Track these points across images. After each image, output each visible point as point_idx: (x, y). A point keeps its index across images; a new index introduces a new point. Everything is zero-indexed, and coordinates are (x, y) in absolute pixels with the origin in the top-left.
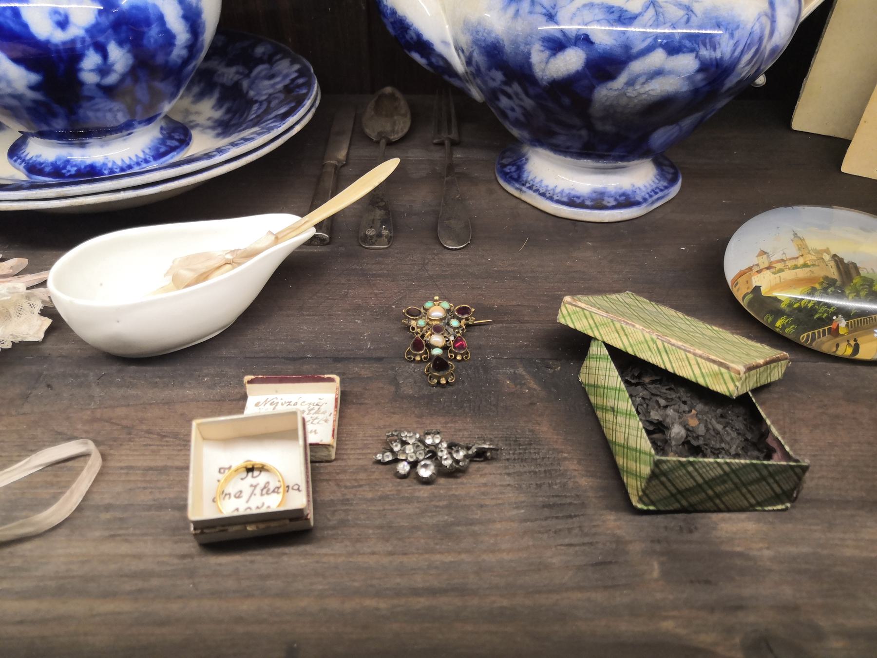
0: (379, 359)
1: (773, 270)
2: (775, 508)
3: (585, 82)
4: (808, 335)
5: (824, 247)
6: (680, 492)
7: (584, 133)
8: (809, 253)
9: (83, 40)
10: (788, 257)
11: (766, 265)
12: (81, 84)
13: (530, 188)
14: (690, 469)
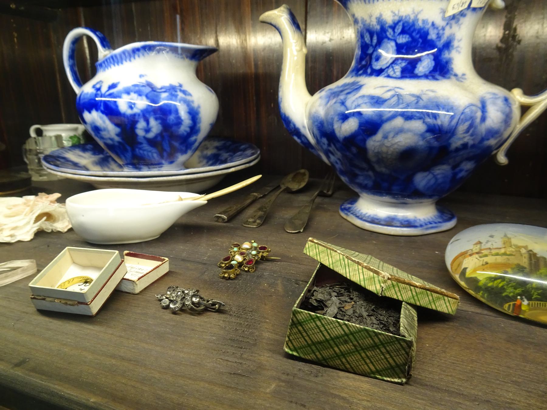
0: (205, 264)
1: (481, 255)
2: (392, 380)
3: (360, 137)
4: (510, 305)
5: (524, 245)
6: (313, 343)
7: (371, 173)
8: (511, 246)
9: (139, 115)
10: (494, 247)
11: (477, 251)
12: (136, 135)
13: (352, 213)
14: (319, 323)
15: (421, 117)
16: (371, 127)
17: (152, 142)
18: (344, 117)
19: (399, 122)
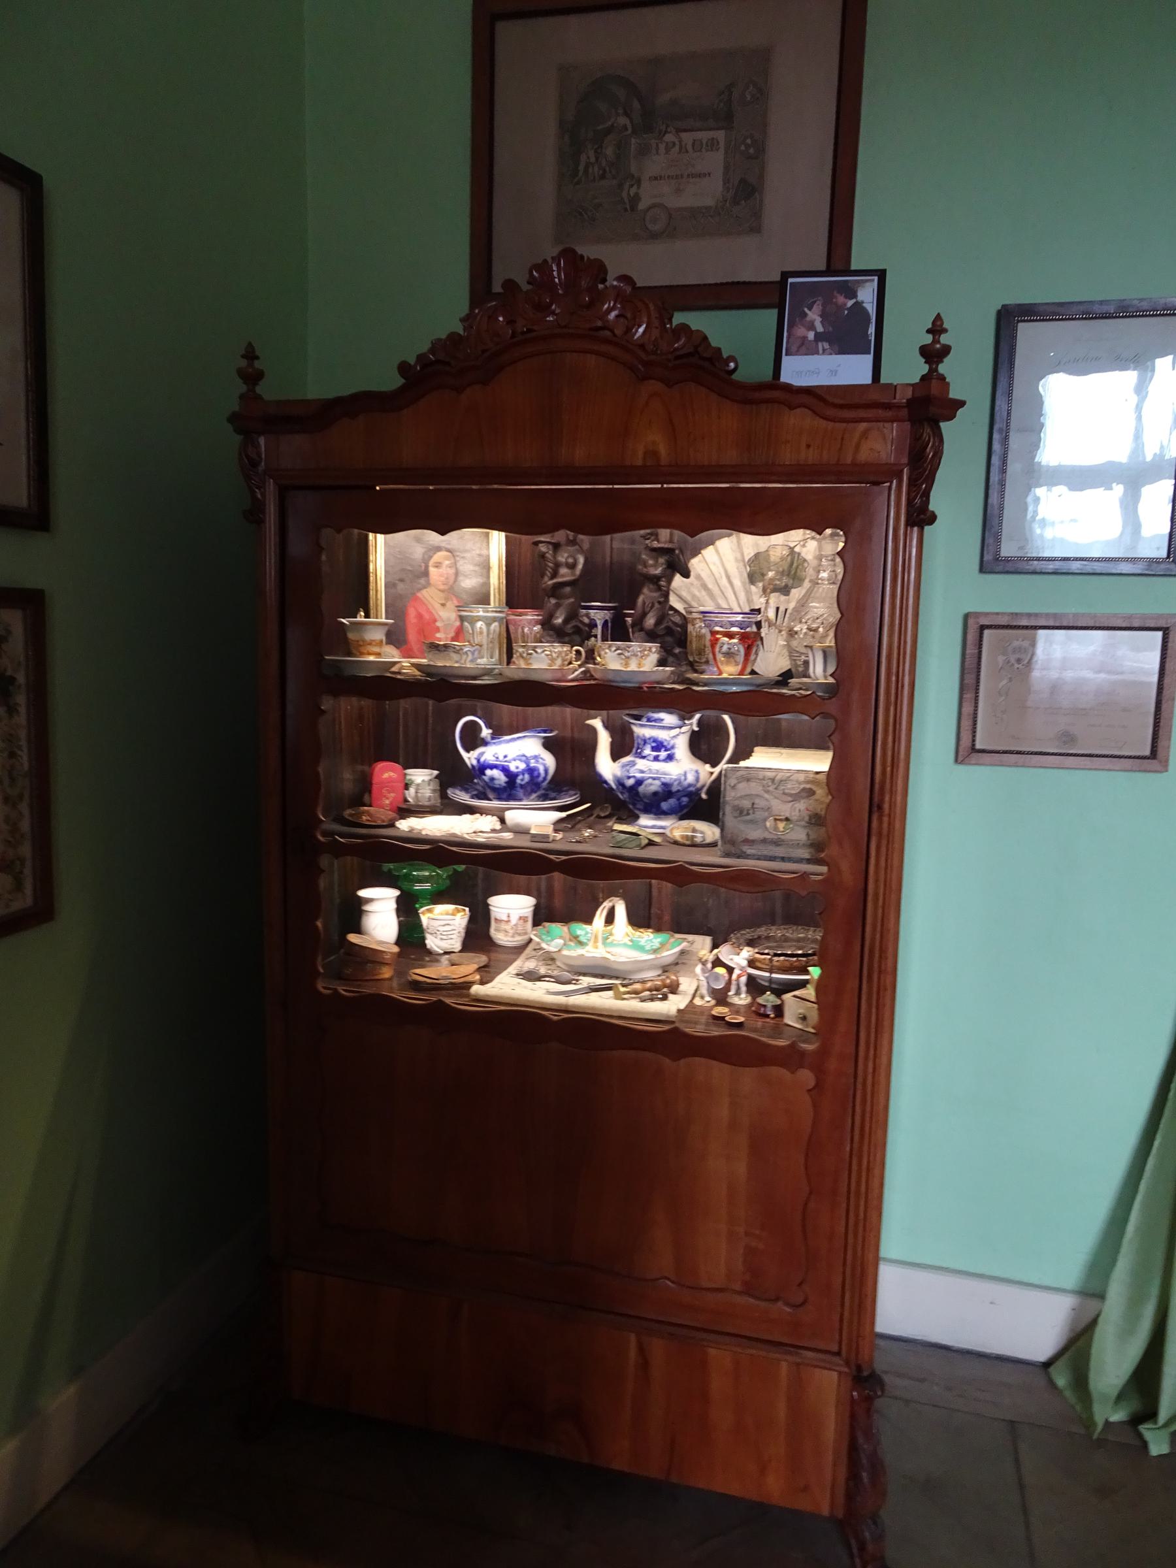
15: (658, 779)
16: (639, 782)
17: (522, 786)
18: (629, 777)
19: (650, 781)
